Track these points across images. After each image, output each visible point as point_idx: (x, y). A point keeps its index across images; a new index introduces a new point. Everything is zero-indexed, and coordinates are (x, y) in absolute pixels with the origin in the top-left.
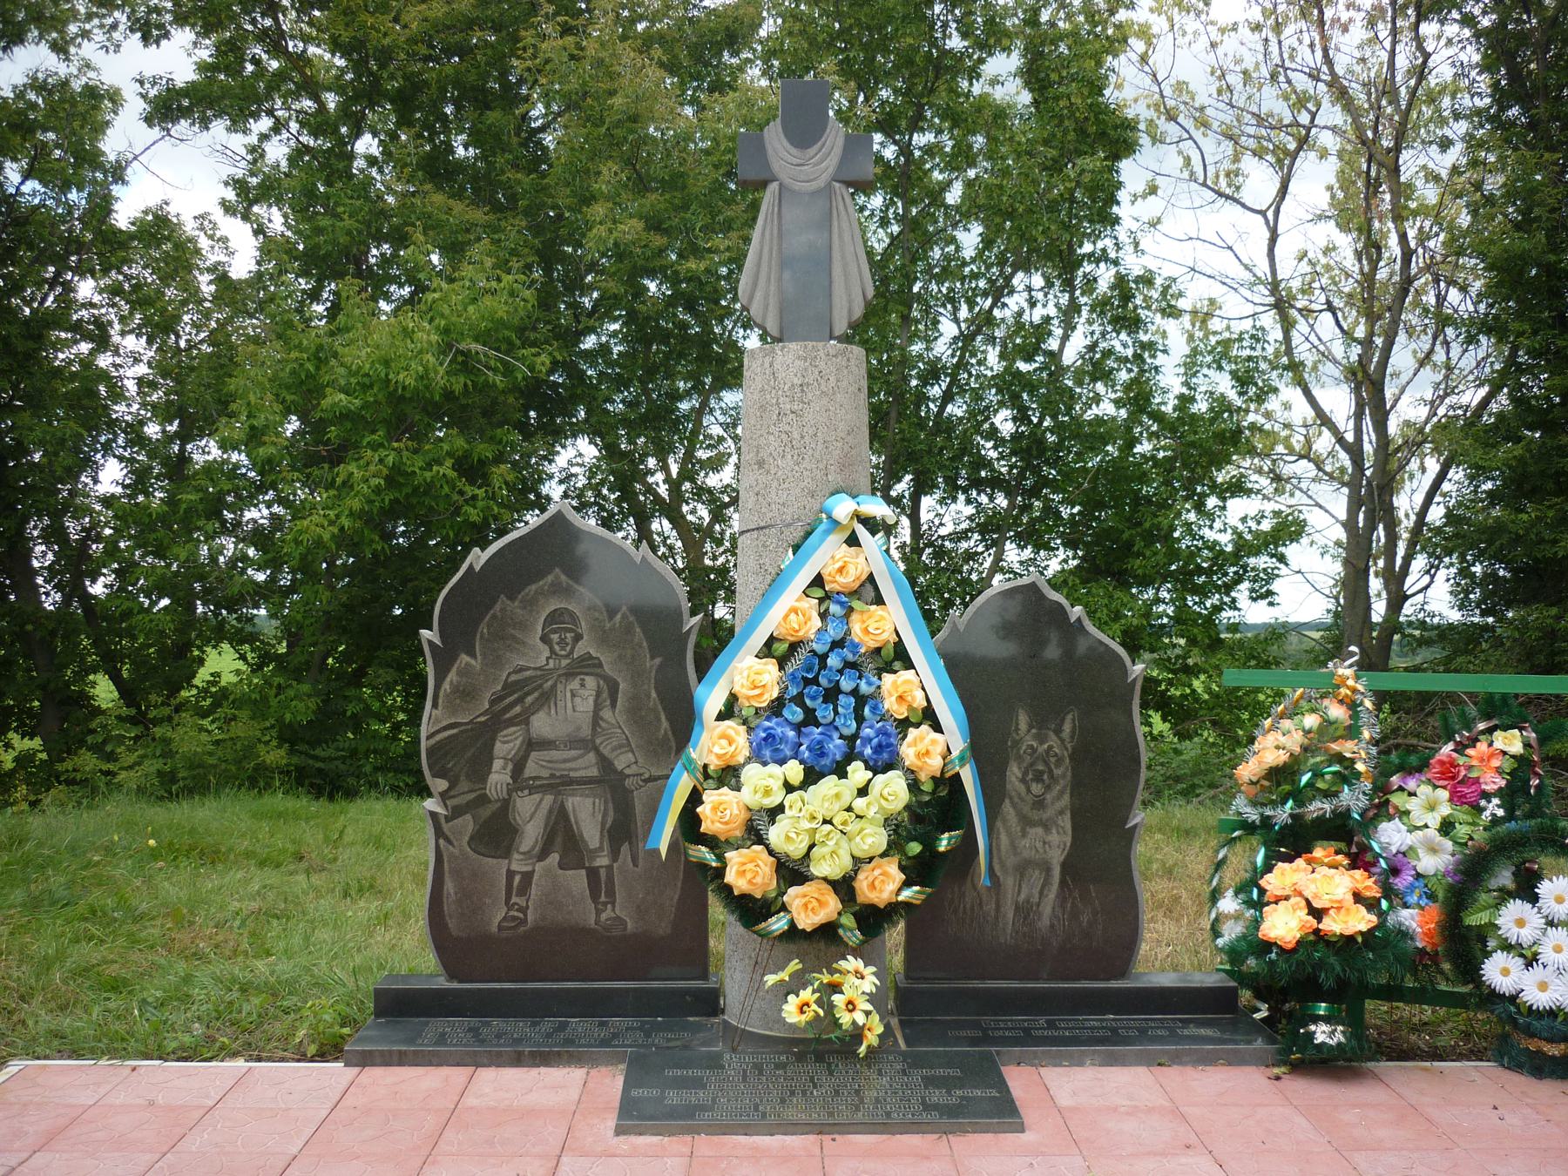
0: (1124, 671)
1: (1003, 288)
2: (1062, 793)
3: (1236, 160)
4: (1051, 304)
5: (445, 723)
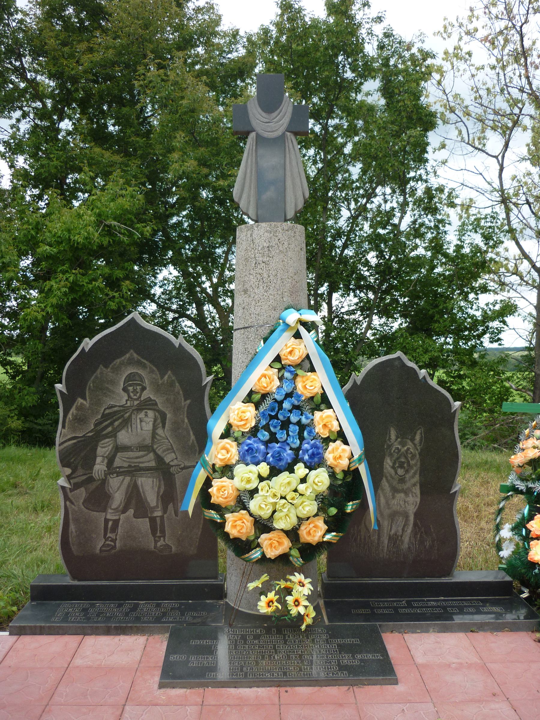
0: (450, 406)
1: (372, 193)
2: (415, 474)
3: (483, 131)
4: (394, 201)
5: (69, 437)
